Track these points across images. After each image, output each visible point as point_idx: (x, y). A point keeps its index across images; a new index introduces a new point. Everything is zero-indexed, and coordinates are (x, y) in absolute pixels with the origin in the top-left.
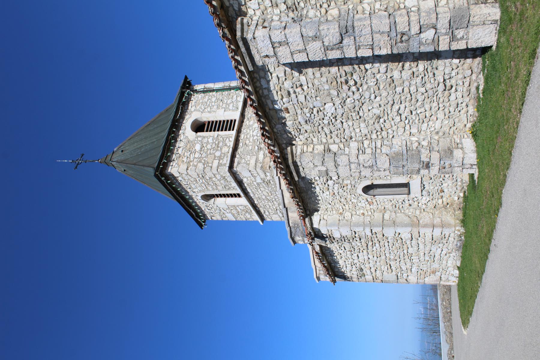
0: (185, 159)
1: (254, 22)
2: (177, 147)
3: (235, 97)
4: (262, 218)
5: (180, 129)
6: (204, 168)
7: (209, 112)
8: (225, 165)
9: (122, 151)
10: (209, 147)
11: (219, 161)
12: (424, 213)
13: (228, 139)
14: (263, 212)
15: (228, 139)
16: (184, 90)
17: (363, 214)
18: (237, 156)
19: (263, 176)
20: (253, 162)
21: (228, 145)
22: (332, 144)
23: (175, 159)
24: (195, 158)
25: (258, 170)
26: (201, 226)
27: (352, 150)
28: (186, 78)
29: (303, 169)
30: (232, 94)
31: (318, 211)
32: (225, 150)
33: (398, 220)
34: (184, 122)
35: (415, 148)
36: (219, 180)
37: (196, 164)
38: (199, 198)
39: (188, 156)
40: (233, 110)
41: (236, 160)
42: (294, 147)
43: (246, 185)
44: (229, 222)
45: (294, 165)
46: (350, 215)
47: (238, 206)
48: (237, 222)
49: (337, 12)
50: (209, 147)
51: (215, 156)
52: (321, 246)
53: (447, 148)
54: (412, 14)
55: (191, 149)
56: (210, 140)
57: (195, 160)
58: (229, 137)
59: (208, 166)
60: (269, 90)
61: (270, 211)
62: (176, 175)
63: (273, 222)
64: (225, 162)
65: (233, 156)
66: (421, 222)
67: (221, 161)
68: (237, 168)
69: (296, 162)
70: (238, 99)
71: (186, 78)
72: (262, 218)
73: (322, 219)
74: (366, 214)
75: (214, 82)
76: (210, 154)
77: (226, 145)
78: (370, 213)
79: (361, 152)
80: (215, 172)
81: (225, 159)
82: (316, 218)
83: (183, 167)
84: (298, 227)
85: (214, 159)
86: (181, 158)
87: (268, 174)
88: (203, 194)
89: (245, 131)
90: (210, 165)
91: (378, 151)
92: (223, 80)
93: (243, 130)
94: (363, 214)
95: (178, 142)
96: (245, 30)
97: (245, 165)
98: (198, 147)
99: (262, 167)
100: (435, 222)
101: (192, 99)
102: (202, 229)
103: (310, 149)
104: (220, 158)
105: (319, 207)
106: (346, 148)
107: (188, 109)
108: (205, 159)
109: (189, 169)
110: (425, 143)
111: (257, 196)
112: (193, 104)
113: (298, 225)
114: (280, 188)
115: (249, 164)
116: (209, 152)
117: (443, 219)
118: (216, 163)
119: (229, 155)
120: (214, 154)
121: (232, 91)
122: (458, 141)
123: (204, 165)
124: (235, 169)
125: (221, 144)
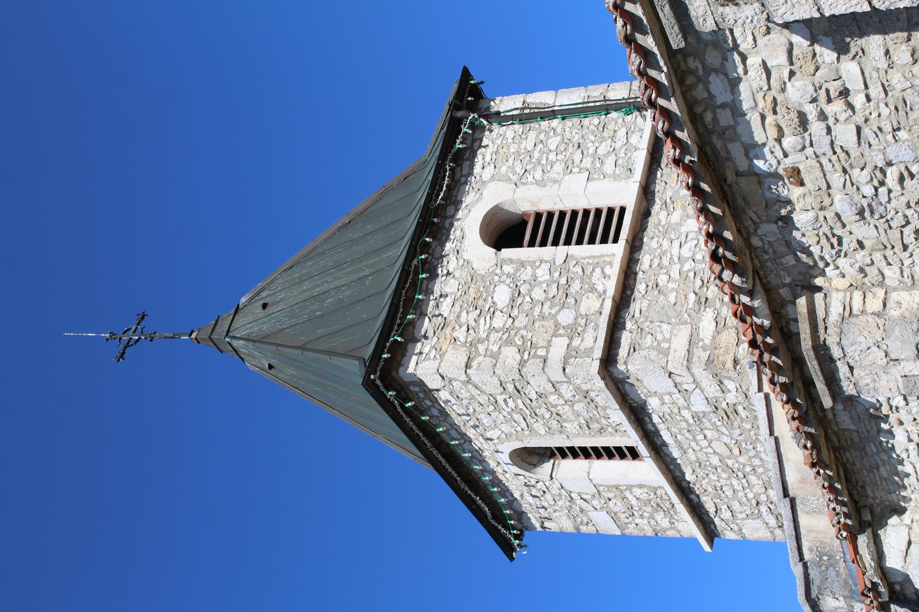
0: (461, 334)
3: (622, 133)
4: (711, 533)
5: (447, 238)
6: (522, 363)
7: (540, 183)
8: (589, 352)
9: (265, 306)
11: (571, 339)
13: (598, 270)
14: (711, 509)
15: (598, 270)
16: (459, 114)
18: (629, 325)
19: (712, 390)
20: (680, 344)
21: (600, 288)
23: (430, 334)
24: (492, 329)
25: (698, 370)
26: (508, 549)
28: (466, 74)
29: (851, 369)
30: (611, 126)
31: (901, 511)
32: (590, 304)
34: (460, 214)
36: (570, 403)
38: (505, 457)
40: (616, 177)
41: (626, 338)
42: (818, 297)
43: (656, 419)
44: (599, 538)
45: (818, 357)
47: (630, 488)
51: (557, 325)
55: (480, 302)
56: (542, 273)
57: (494, 336)
58: (601, 263)
60: (737, 112)
61: (736, 506)
62: (433, 382)
63: (744, 544)
67: (576, 342)
68: (629, 364)
70: (634, 140)
71: (466, 74)
72: (711, 533)
75: (555, 86)
76: (543, 317)
77: (593, 289)
80: (558, 376)
81: (589, 335)
82: (893, 535)
83: (455, 359)
84: (832, 563)
85: (555, 335)
86: (448, 330)
87: (730, 385)
88: (518, 445)
89: (654, 244)
90: (541, 352)
92: (585, 83)
93: (650, 241)
98: (502, 295)
99: (709, 362)
101: (485, 142)
102: (512, 559)
103: (874, 304)
104: (573, 331)
105: (906, 499)
107: (471, 173)
108: (523, 332)
109: (474, 364)
111: (691, 456)
112: (488, 158)
113: (831, 557)
114: (771, 433)
116: (537, 310)
118: (559, 346)
119: (603, 322)
120: (554, 317)
121: (614, 115)
124: (621, 367)
125: (576, 286)
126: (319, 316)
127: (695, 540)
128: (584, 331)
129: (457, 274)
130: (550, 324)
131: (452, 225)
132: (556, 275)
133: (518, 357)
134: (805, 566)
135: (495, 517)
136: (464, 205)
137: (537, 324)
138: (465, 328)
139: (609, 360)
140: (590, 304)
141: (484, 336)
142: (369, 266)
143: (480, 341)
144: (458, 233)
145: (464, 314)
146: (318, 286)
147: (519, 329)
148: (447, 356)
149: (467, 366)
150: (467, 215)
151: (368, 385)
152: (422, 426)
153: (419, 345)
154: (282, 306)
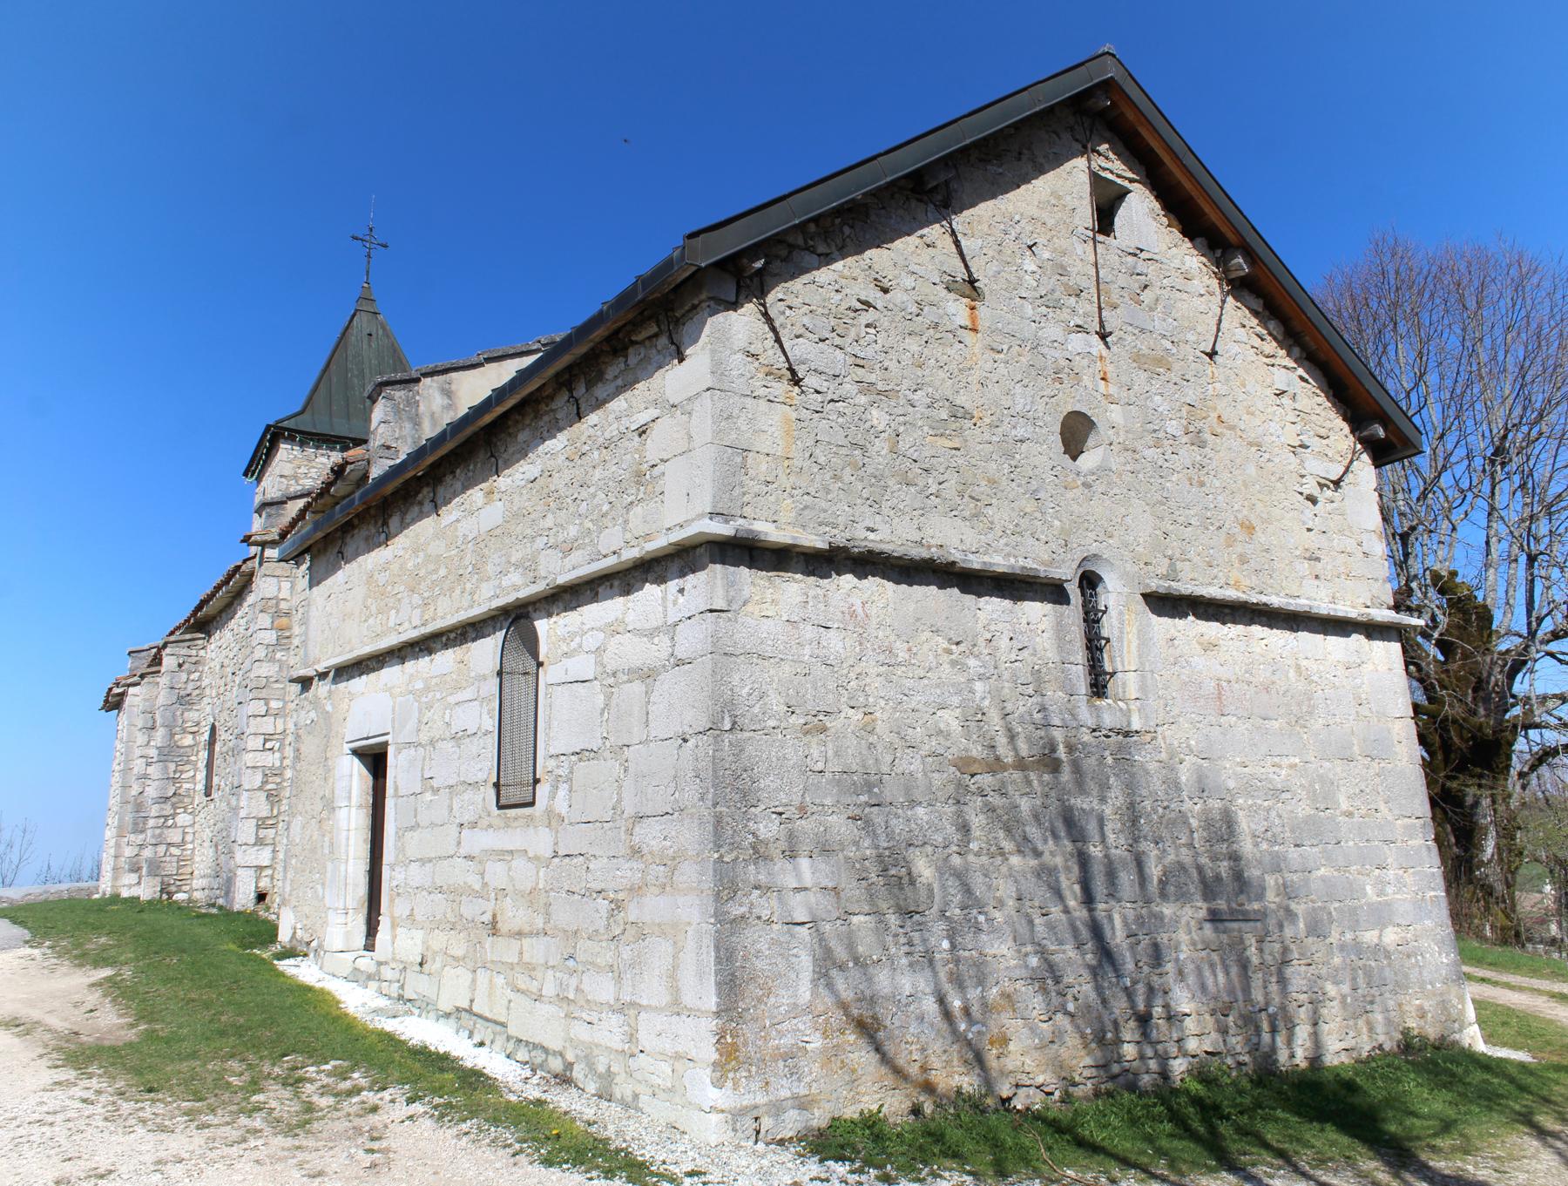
1: (194, 652)
83: (288, 469)
151: (268, 427)
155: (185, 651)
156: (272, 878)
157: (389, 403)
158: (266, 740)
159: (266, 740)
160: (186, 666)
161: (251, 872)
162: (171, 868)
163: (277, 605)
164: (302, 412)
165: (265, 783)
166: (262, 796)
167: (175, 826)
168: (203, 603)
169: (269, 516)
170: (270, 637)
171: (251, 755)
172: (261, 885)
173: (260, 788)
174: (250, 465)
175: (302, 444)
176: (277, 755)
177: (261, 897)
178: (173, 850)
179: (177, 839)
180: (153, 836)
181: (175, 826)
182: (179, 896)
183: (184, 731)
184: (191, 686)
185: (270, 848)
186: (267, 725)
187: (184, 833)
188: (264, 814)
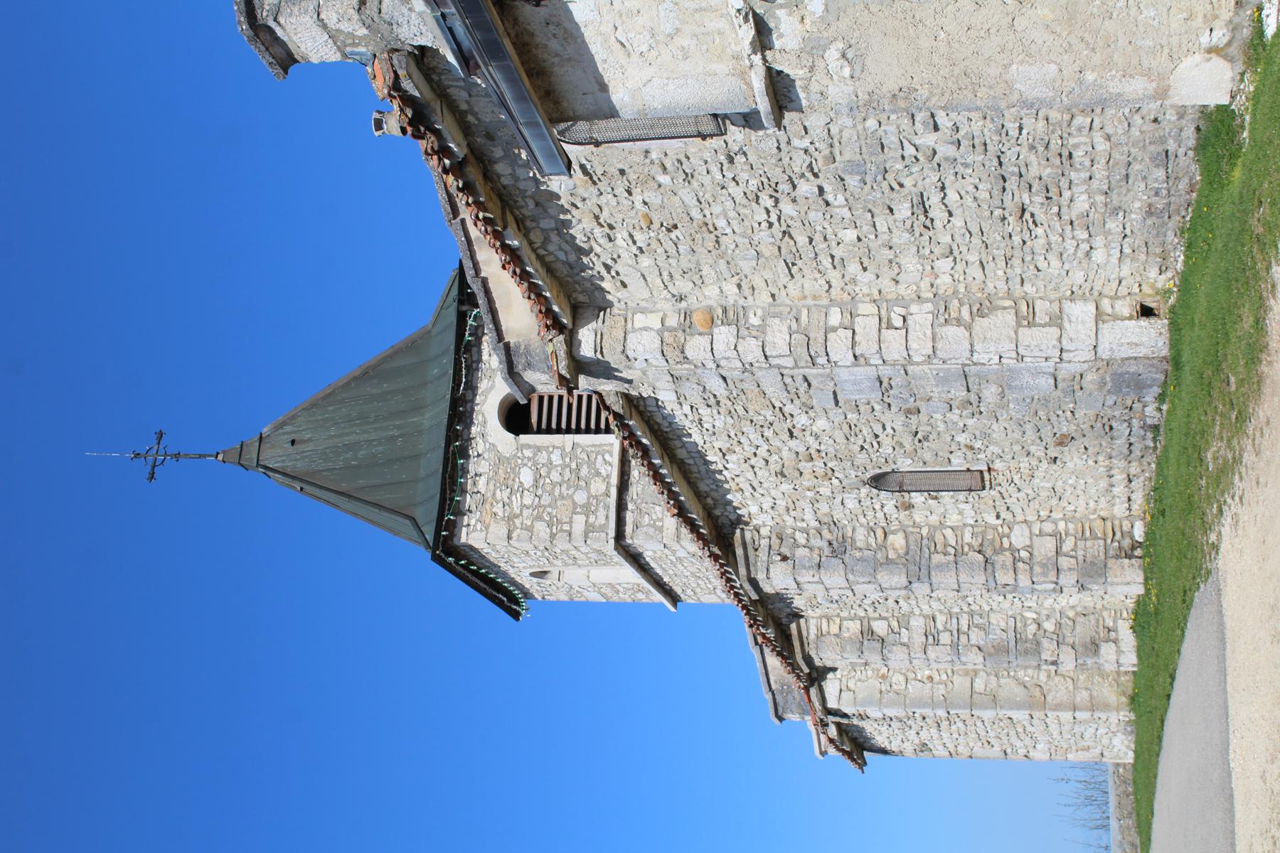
0: (498, 509)
1: (764, 542)
2: (472, 473)
8: (602, 529)
9: (293, 442)
10: (555, 476)
11: (588, 517)
12: (1057, 679)
13: (600, 457)
15: (600, 457)
16: (464, 308)
17: (930, 678)
18: (630, 506)
21: (603, 472)
22: (875, 619)
23: (473, 508)
24: (523, 506)
27: (915, 636)
32: (598, 487)
33: (1002, 694)
34: (478, 399)
35: (1031, 637)
37: (529, 523)
39: (506, 500)
41: (629, 517)
42: (802, 621)
46: (902, 679)
48: (608, 603)
49: (903, 542)
50: (555, 476)
51: (574, 504)
52: (838, 725)
53: (1088, 640)
54: (1020, 565)
55: (510, 482)
56: (556, 458)
57: (526, 513)
59: (562, 530)
63: (701, 606)
64: (601, 520)
65: (621, 507)
66: (1049, 698)
67: (592, 519)
68: (635, 540)
69: (810, 657)
73: (844, 688)
74: (936, 678)
76: (562, 497)
77: (598, 474)
78: (944, 677)
79: (930, 638)
83: (498, 530)
84: (790, 692)
85: (574, 513)
86: (488, 506)
90: (566, 527)
91: (963, 639)
94: (930, 678)
95: (472, 460)
96: (751, 559)
97: (651, 530)
98: (526, 477)
100: (1078, 699)
103: (835, 629)
104: (587, 510)
106: (903, 630)
107: (480, 360)
108: (549, 510)
109: (514, 535)
110: (1049, 626)
113: (789, 687)
115: (661, 530)
117: (1095, 694)
118: (579, 520)
120: (571, 497)
122: (1111, 624)
123: (550, 525)
124: (629, 541)
125: (584, 471)
126: (355, 466)
127: (661, 604)
128: (597, 510)
129: (486, 456)
130: (569, 503)
131: (473, 410)
132: (568, 460)
133: (548, 530)
134: (773, 694)
135: (509, 600)
136: (480, 391)
137: (559, 503)
138: (501, 505)
139: (620, 535)
140: (598, 487)
141: (518, 512)
142: (398, 427)
143: (517, 516)
144: (480, 418)
145: (498, 492)
146: (347, 434)
147: (545, 507)
148: (492, 529)
149: (509, 538)
150: (485, 401)
151: (436, 559)
152: (475, 573)
153: (466, 518)
154: (310, 447)
155: (763, 555)
156: (1116, 297)
157: (285, 10)
158: (890, 326)
159: (890, 326)
160: (785, 551)
161: (1105, 328)
162: (1095, 548)
163: (671, 330)
164: (413, 520)
165: (959, 322)
166: (980, 324)
167: (1030, 548)
168: (682, 513)
169: (529, 365)
170: (724, 335)
171: (913, 345)
172: (1126, 312)
173: (969, 328)
174: (500, 604)
175: (460, 513)
176: (914, 308)
177: (1146, 312)
178: (1068, 545)
179: (1050, 544)
180: (1044, 574)
181: (1030, 548)
182: (1139, 533)
183: (883, 547)
184: (817, 542)
185: (1067, 305)
186: (866, 325)
187: (1041, 534)
188: (1010, 318)
